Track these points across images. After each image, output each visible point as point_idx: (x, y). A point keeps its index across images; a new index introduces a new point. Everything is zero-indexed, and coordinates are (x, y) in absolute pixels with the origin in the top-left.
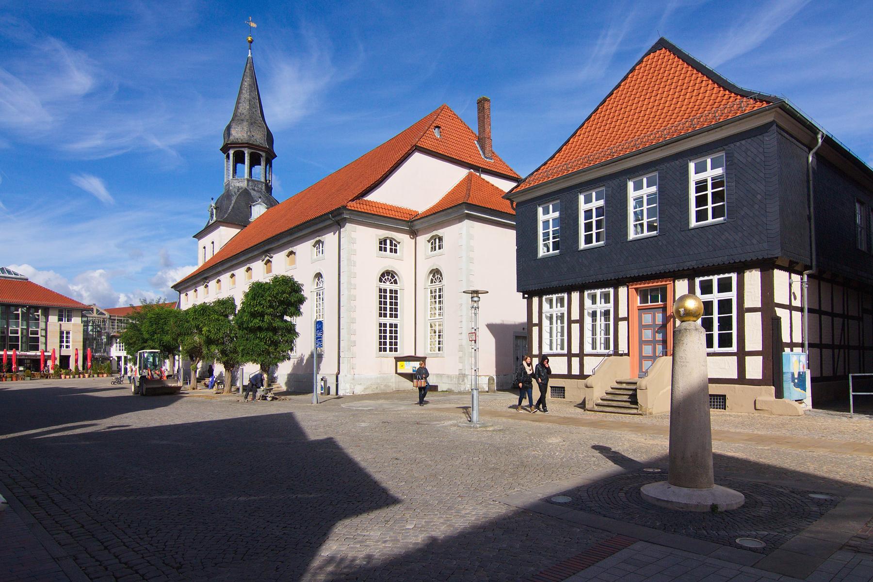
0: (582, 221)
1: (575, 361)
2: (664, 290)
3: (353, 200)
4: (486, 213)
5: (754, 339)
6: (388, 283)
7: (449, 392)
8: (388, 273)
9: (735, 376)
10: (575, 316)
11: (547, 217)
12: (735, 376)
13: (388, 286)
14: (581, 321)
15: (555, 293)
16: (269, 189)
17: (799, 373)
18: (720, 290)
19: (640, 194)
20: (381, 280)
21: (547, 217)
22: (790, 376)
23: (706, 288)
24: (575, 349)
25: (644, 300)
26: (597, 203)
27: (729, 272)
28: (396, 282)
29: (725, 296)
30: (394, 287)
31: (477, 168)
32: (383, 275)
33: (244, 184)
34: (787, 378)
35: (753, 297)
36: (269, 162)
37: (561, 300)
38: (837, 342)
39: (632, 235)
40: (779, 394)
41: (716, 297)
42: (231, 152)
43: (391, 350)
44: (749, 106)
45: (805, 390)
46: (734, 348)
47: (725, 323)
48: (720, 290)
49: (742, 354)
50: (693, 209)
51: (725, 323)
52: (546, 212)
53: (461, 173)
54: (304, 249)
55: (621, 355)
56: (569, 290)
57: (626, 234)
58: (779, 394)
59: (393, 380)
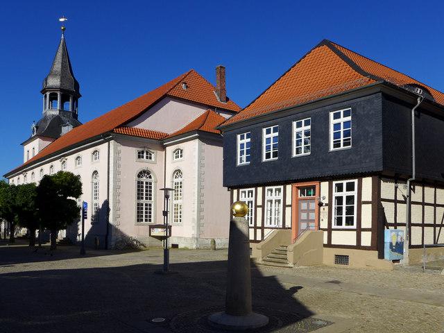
0: (264, 145)
1: (259, 231)
2: (314, 187)
3: (118, 127)
4: (207, 137)
5: (367, 222)
6: (144, 178)
7: (185, 249)
8: (144, 172)
9: (355, 244)
10: (260, 203)
11: (242, 141)
12: (355, 244)
13: (144, 179)
14: (263, 206)
15: (247, 188)
16: (75, 116)
17: (397, 243)
18: (348, 190)
19: (300, 130)
20: (139, 176)
21: (242, 141)
22: (388, 245)
23: (340, 188)
24: (259, 224)
25: (302, 193)
26: (273, 135)
27: (280, 185)
28: (150, 177)
29: (350, 193)
30: (149, 180)
31: (212, 108)
32: (141, 173)
33: (56, 113)
34: (387, 246)
35: (367, 194)
36: (75, 100)
37: (279, 190)
38: (438, 222)
39: (294, 155)
40: (381, 256)
41: (345, 194)
42: (48, 94)
43: (146, 220)
44: (374, 82)
45: (402, 253)
46: (355, 226)
47: (350, 211)
48: (348, 190)
49: (359, 230)
50: (264, 152)
51: (350, 211)
52: (242, 138)
53: (202, 112)
54: (86, 154)
55: (287, 228)
56: (256, 186)
57: (291, 153)
58: (381, 256)
59: (148, 240)
